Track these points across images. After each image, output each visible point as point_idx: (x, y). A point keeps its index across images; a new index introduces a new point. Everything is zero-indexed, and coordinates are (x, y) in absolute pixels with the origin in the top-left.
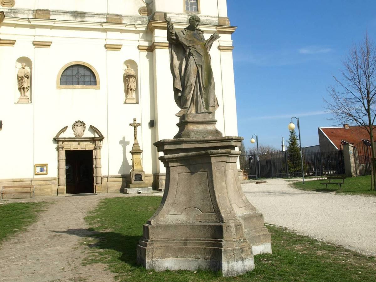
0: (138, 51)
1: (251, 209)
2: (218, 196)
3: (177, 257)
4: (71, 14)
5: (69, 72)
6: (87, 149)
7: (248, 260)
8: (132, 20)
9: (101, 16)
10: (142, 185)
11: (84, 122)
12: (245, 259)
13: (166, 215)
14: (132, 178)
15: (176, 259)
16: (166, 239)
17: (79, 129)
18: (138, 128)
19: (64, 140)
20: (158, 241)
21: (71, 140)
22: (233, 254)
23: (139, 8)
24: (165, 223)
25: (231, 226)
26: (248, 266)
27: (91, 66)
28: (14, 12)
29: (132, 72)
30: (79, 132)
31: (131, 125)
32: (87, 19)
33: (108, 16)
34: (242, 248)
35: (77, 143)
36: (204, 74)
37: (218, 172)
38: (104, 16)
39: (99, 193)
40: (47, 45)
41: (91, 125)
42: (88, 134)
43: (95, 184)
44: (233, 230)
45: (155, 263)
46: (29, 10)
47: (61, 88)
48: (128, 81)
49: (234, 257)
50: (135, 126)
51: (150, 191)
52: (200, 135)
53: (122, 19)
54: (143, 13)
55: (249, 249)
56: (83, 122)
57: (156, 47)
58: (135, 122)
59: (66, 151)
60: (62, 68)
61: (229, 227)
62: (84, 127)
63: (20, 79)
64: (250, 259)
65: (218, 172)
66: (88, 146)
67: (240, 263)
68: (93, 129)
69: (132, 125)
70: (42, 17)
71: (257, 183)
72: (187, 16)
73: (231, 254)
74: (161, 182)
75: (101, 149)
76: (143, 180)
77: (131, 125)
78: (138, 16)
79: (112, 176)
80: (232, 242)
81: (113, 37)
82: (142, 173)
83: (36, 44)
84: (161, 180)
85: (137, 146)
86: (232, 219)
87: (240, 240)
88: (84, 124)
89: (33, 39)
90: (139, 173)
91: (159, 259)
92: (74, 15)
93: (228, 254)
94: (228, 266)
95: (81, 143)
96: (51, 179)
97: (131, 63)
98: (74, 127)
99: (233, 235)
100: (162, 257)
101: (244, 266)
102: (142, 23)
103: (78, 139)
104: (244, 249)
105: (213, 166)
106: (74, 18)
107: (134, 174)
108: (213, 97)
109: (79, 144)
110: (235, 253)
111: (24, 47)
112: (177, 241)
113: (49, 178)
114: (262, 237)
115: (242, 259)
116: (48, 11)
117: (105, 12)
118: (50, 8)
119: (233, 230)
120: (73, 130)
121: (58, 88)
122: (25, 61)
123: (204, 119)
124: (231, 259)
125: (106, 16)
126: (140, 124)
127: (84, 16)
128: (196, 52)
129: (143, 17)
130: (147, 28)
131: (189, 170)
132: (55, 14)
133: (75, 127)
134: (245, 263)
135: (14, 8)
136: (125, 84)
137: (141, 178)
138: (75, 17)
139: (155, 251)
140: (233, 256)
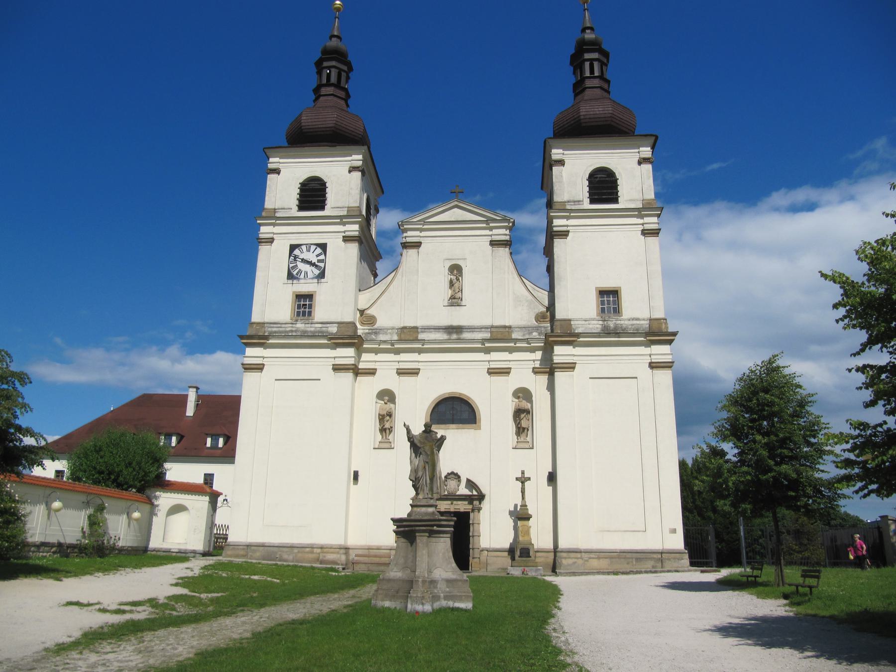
6: (462, 510)
27: (469, 398)
28: (376, 333)
29: (525, 405)
30: (452, 487)
31: (517, 479)
32: (466, 335)
40: (415, 372)
41: (392, 519)
42: (463, 490)
43: (471, 559)
44: (420, 584)
46: (393, 328)
50: (523, 480)
53: (512, 332)
63: (382, 418)
66: (462, 507)
68: (470, 484)
71: (702, 572)
72: (601, 322)
77: (517, 479)
81: (499, 358)
82: (530, 547)
83: (401, 372)
88: (459, 477)
89: (397, 366)
95: (455, 502)
97: (523, 394)
100: (382, 600)
107: (520, 546)
111: (386, 378)
115: (423, 604)
116: (416, 328)
117: (488, 323)
118: (419, 324)
119: (420, 584)
122: (387, 396)
126: (529, 479)
127: (461, 332)
135: (375, 327)
136: (515, 421)
138: (450, 333)
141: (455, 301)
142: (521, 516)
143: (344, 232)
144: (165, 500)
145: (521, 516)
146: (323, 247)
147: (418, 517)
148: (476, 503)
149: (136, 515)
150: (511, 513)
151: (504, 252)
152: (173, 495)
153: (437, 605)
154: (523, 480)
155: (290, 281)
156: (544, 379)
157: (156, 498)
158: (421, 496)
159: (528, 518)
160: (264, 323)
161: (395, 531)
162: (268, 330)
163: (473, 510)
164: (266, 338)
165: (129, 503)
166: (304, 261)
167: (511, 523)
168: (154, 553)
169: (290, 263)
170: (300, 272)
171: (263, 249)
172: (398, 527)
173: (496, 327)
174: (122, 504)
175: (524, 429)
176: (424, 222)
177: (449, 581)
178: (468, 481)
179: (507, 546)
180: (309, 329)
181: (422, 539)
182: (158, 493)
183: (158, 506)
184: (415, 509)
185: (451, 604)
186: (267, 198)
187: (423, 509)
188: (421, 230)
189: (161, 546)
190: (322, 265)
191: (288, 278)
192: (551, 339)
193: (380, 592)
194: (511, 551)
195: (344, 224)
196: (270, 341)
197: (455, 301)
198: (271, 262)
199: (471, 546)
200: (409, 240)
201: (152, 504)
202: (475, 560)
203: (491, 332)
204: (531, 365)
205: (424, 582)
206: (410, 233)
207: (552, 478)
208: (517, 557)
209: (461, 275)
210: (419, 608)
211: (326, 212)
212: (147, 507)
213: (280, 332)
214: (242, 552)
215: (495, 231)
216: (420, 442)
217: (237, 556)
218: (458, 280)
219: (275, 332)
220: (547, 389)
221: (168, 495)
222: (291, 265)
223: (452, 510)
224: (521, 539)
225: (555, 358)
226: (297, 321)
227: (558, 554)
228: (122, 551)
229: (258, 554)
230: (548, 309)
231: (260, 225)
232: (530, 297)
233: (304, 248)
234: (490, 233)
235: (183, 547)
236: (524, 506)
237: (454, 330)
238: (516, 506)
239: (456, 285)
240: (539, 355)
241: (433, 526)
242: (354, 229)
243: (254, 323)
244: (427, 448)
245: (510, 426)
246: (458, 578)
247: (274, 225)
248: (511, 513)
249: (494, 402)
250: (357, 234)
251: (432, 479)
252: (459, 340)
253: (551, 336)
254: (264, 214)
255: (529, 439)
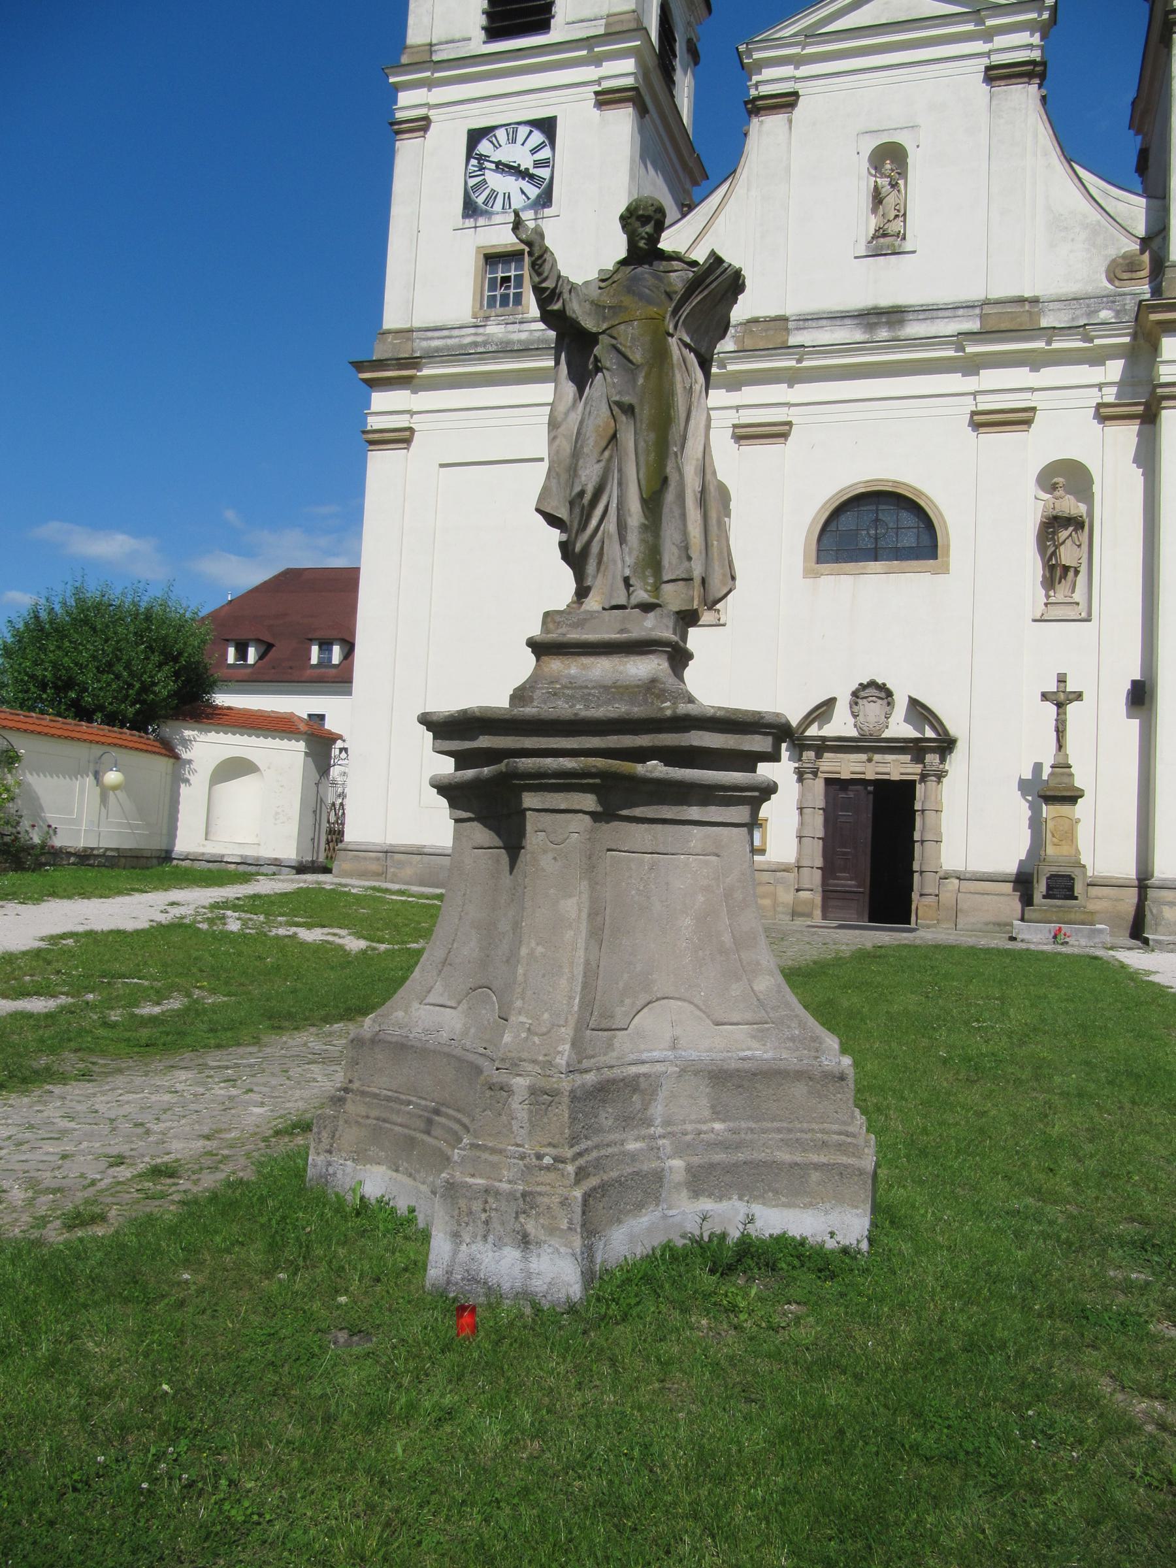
0: (1096, 426)
1: (792, 1039)
2: (531, 954)
3: (397, 1171)
4: (856, 322)
5: (847, 521)
6: (895, 777)
7: (549, 1251)
8: (1078, 312)
9: (960, 312)
10: (1072, 916)
11: (888, 686)
12: (539, 1244)
13: (416, 1005)
14: (1036, 885)
15: (394, 1174)
16: (390, 1093)
17: (872, 710)
18: (1071, 708)
19: (823, 746)
20: (363, 1094)
21: (843, 746)
22: (485, 1211)
23: (1107, 263)
24: (404, 1032)
25: (514, 1088)
26: (548, 1280)
27: (920, 493)
29: (1071, 506)
30: (872, 719)
31: (1045, 696)
32: (914, 329)
33: (987, 310)
34: (531, 1193)
35: (864, 757)
36: (645, 441)
37: (550, 855)
38: (971, 312)
39: (928, 927)
40: (778, 433)
42: (899, 727)
43: (915, 896)
44: (519, 1107)
45: (335, 1174)
47: (817, 575)
48: (1053, 539)
49: (487, 1223)
50: (1061, 699)
51: (1097, 940)
52: (572, 697)
53: (1042, 311)
54: (1125, 276)
55: (562, 1204)
56: (884, 685)
57: (1165, 404)
58: (1062, 685)
59: (829, 782)
60: (822, 507)
61: (502, 1089)
62: (889, 704)
64: (562, 1250)
65: (550, 855)
66: (897, 767)
67: (511, 1254)
68: (919, 711)
69: (1048, 696)
70: (761, 345)
73: (474, 1208)
74: (1154, 911)
75: (944, 780)
76: (1076, 898)
77: (1045, 696)
78: (1105, 293)
79: (974, 873)
80: (495, 1158)
81: (1002, 385)
82: (1075, 873)
84: (1154, 902)
85: (1062, 774)
86: (534, 1062)
87: (539, 1157)
90: (1062, 869)
91: (348, 1163)
92: (865, 322)
93: (462, 1203)
94: (455, 1253)
95: (877, 757)
96: (774, 867)
97: (1068, 477)
98: (856, 704)
99: (515, 1128)
100: (360, 1156)
101: (529, 1275)
102: (1117, 316)
103: (868, 744)
104: (539, 1200)
105: (529, 827)
106: (864, 332)
107: (1047, 871)
108: (677, 537)
109: (870, 760)
110: (494, 1206)
112: (416, 1111)
113: (769, 863)
114: (815, 1176)
115: (525, 1242)
116: (784, 319)
117: (976, 293)
118: (791, 309)
119: (519, 1107)
120: (852, 712)
121: (808, 573)
123: (622, 631)
124: (470, 1228)
125: (977, 311)
126: (1079, 696)
127: (901, 322)
128: (614, 354)
129: (1125, 294)
130: (1135, 336)
131: (496, 838)
132: (805, 328)
133: (860, 701)
134: (534, 1259)
137: (1072, 889)
138: (871, 327)
139: (340, 1128)
140: (484, 1216)
141: (886, 242)
142: (1053, 792)
143: (598, 82)
144: (205, 748)
145: (1053, 792)
146: (547, 126)
147: (562, 709)
148: (932, 759)
149: (112, 777)
150: (1024, 786)
151: (1024, 98)
152: (221, 737)
153: (629, 1238)
154: (1061, 699)
155: (470, 222)
156: (1127, 435)
157: (186, 743)
158: (593, 603)
159: (1072, 798)
160: (411, 331)
161: (444, 789)
162: (421, 345)
163: (924, 777)
164: (413, 362)
165: (97, 750)
166: (503, 168)
167: (1022, 810)
168: (187, 863)
169: (469, 175)
170: (493, 195)
171: (407, 150)
172: (463, 760)
173: (998, 302)
174: (81, 752)
175: (1066, 569)
176: (810, 35)
177: (728, 1081)
178: (914, 703)
179: (1012, 868)
180: (515, 337)
181: (559, 830)
182: (187, 733)
183: (190, 762)
184: (555, 665)
185: (732, 1216)
186: (411, 21)
187: (601, 668)
188: (797, 61)
189: (201, 850)
190: (544, 173)
191: (466, 215)
192: (1154, 317)
193: (353, 1107)
194: (1023, 882)
195: (597, 61)
196: (426, 372)
197: (886, 242)
198: (425, 178)
199: (916, 866)
200: (765, 90)
201: (177, 757)
202: (927, 900)
203: (982, 317)
204: (1093, 397)
205: (542, 1097)
206: (768, 73)
207: (1141, 696)
208: (1038, 898)
209: (903, 174)
210: (501, 1265)
211: (557, 33)
212: (162, 764)
213: (448, 348)
214: (374, 867)
215: (1000, 41)
216: (598, 306)
217: (363, 875)
218: (894, 185)
219: (437, 349)
220: (1136, 460)
221: (212, 736)
222: (472, 182)
223: (870, 776)
224: (1050, 850)
225: (1163, 369)
226: (487, 318)
227: (1151, 893)
228: (85, 858)
229: (408, 872)
230: (1145, 242)
231: (396, 88)
232: (1095, 216)
233: (501, 134)
234: (986, 47)
235: (251, 852)
236: (1063, 766)
237: (884, 317)
238: (1038, 767)
239: (890, 201)
240: (1115, 369)
241: (641, 755)
242: (622, 70)
243: (389, 332)
244: (632, 337)
245: (1032, 566)
246: (789, 1058)
247: (430, 84)
248: (1024, 786)
249: (986, 501)
250: (629, 81)
251: (653, 503)
252: (897, 343)
253: (1154, 309)
254: (405, 60)
255: (1078, 596)
